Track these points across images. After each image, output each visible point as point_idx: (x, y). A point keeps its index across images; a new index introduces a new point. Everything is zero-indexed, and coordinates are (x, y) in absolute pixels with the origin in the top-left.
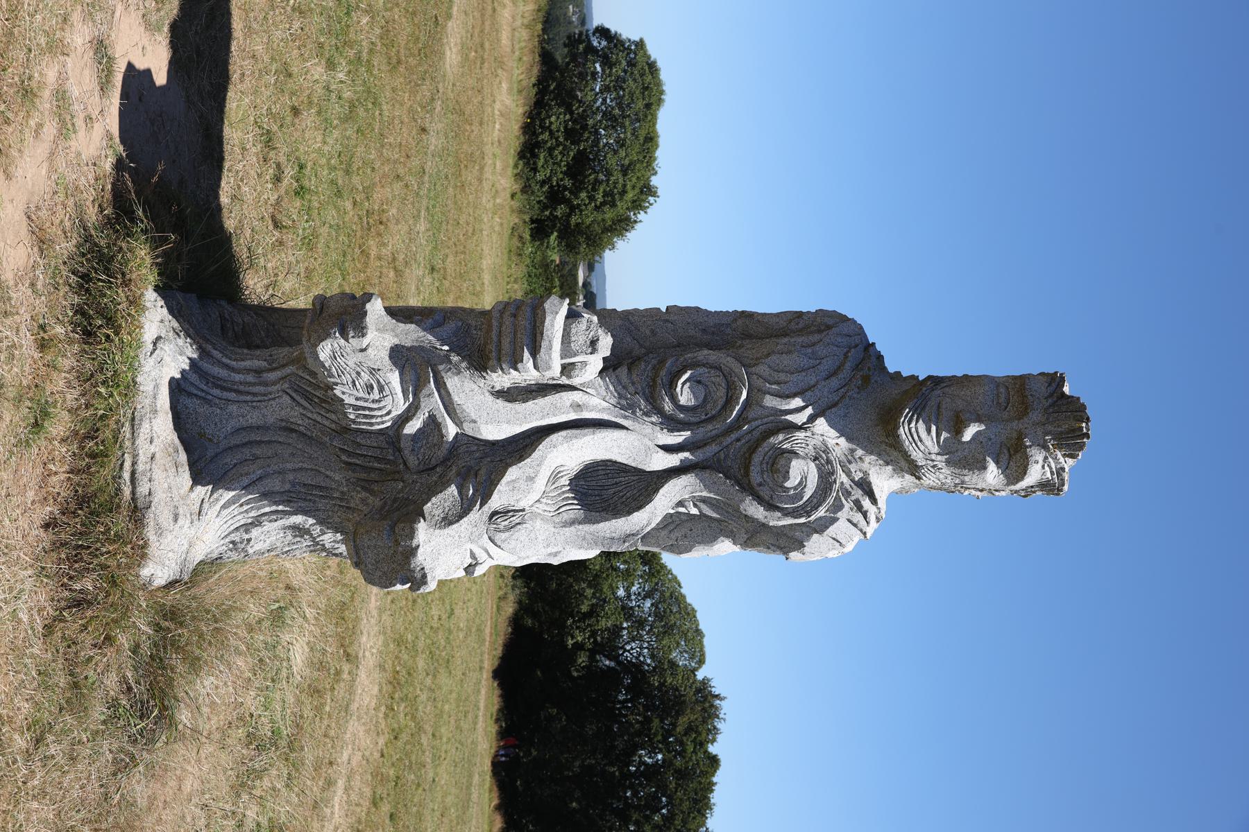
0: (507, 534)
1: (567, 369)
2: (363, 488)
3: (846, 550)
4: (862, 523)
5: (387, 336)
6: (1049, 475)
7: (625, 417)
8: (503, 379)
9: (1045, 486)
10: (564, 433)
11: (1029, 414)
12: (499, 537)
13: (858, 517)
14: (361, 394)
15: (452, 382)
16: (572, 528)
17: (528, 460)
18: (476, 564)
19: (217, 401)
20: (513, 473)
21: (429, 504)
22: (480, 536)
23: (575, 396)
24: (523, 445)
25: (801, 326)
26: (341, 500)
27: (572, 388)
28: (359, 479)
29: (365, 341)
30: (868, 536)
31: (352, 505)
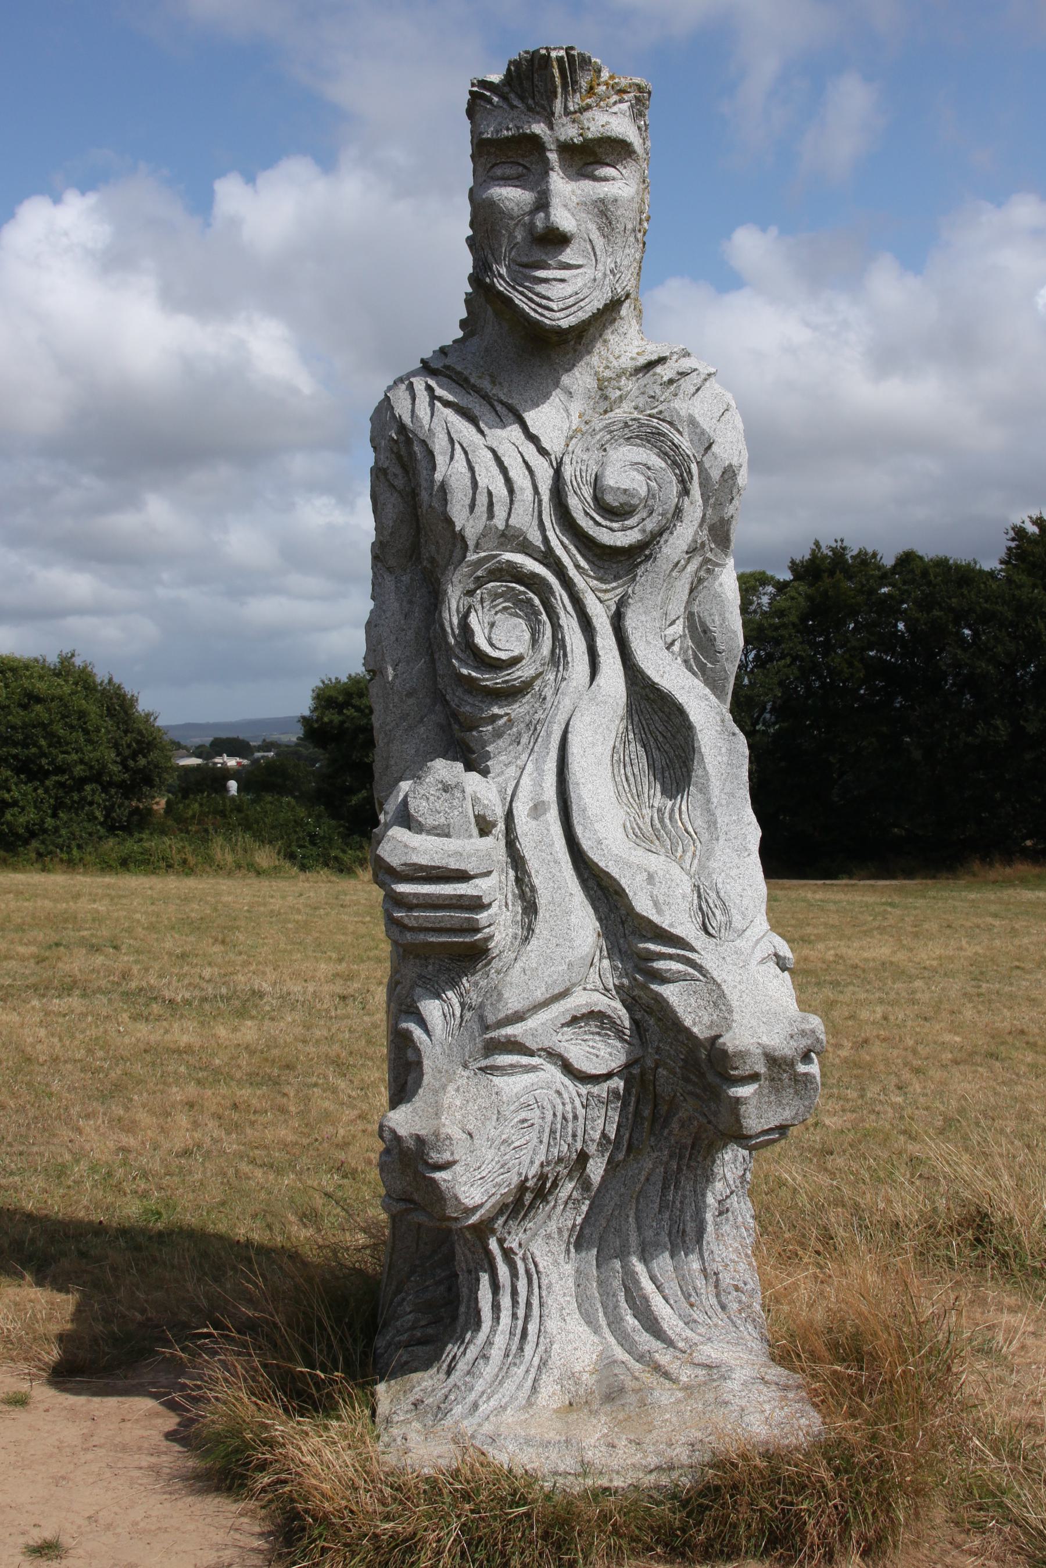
0: (733, 911)
1: (484, 827)
2: (663, 1127)
3: (733, 404)
4: (694, 379)
5: (446, 1102)
6: (625, 106)
7: (549, 735)
8: (500, 923)
9: (638, 110)
10: (579, 830)
11: (521, 120)
12: (738, 922)
13: (687, 385)
14: (534, 1135)
15: (513, 1002)
16: (718, 812)
17: (623, 882)
18: (776, 955)
19: (542, 1348)
20: (643, 905)
21: (695, 1030)
22: (738, 952)
23: (521, 811)
24: (601, 888)
25: (398, 471)
26: (681, 1158)
27: (509, 816)
28: (652, 1132)
29: (456, 1133)
30: (712, 370)
31: (689, 1142)
